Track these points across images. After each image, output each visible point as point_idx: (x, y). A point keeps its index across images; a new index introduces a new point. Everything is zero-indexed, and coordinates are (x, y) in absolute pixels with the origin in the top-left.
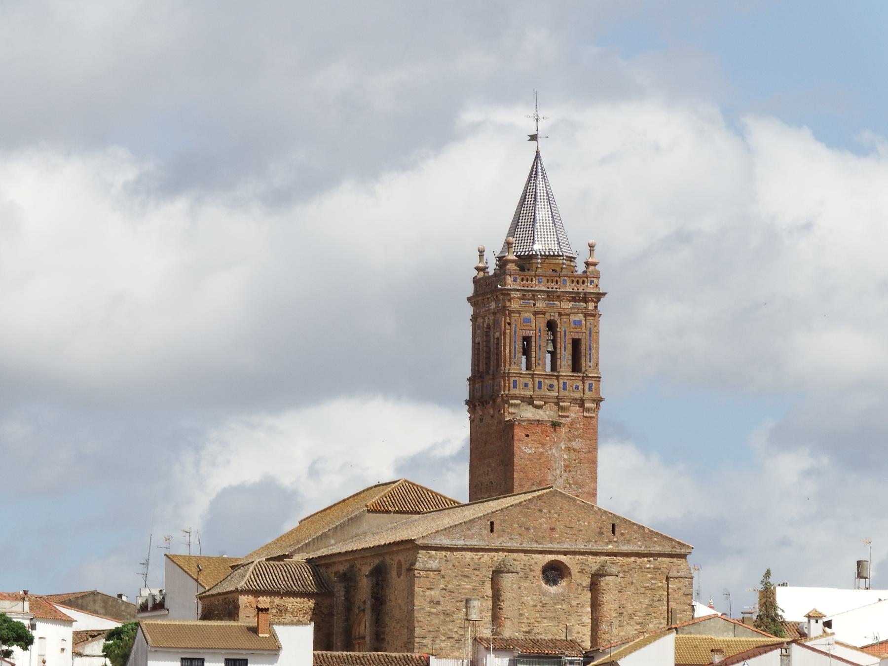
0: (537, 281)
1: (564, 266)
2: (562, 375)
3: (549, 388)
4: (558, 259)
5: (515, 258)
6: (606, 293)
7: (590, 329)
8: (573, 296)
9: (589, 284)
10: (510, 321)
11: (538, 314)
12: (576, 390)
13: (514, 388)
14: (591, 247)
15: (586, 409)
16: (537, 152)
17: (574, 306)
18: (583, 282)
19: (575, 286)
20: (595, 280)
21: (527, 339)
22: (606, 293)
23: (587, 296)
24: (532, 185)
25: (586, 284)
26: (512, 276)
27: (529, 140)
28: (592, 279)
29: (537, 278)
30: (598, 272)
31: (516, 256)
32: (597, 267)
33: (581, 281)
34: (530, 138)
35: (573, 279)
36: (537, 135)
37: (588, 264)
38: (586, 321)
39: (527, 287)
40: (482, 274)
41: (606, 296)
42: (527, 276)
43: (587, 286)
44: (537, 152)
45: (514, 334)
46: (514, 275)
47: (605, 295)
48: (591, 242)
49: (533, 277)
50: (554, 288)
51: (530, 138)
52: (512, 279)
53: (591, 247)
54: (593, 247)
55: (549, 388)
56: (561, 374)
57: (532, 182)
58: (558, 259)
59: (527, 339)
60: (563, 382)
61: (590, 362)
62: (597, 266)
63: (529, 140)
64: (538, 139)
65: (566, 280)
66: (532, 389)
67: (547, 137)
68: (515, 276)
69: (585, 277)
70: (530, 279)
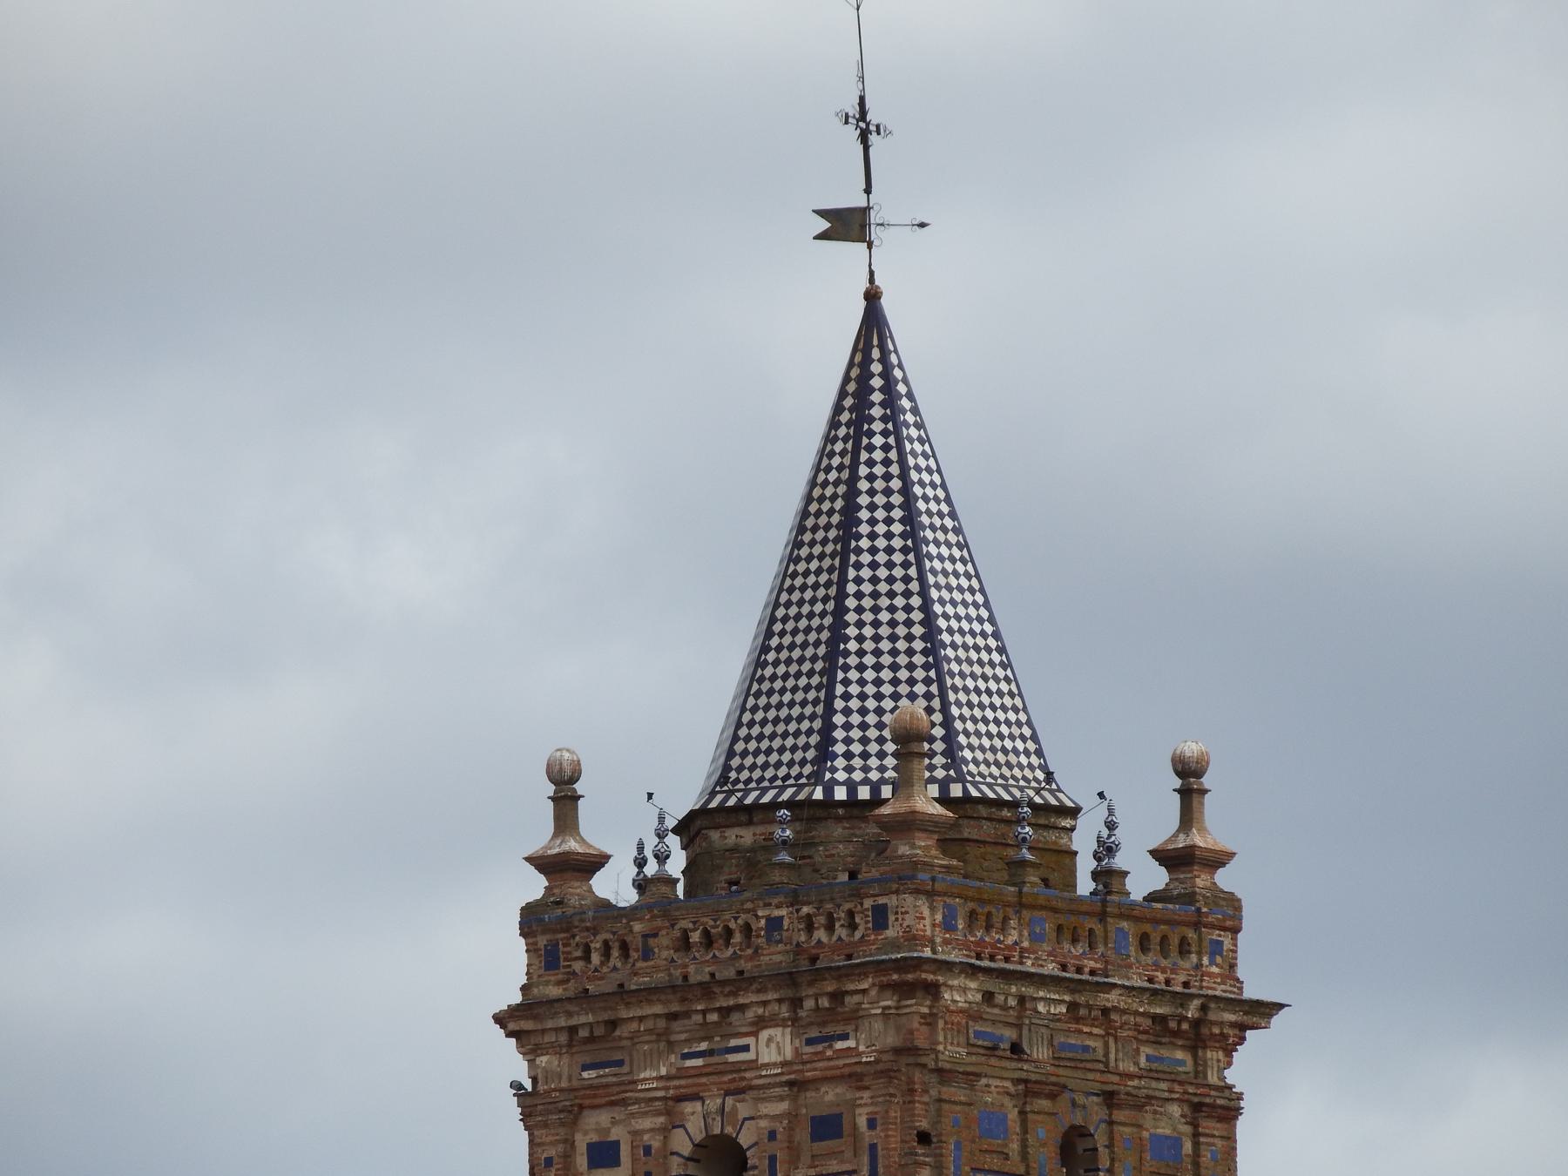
5: (938, 809)
8: (1159, 1011)
9: (1205, 961)
10: (936, 1123)
14: (1189, 775)
16: (872, 297)
18: (1184, 949)
19: (1157, 966)
23: (1212, 1016)
24: (878, 455)
25: (1194, 957)
26: (939, 904)
27: (823, 236)
28: (1215, 935)
29: (1026, 914)
33: (1176, 941)
34: (824, 225)
35: (1148, 928)
36: (868, 208)
38: (1196, 1145)
40: (767, 901)
41: (1277, 1020)
42: (990, 902)
44: (872, 297)
46: (945, 894)
47: (1271, 1016)
48: (1191, 749)
49: (1010, 911)
51: (824, 225)
52: (939, 917)
53: (1189, 775)
54: (1199, 774)
57: (878, 441)
63: (823, 236)
64: (874, 233)
67: (922, 225)
68: (948, 900)
70: (997, 920)
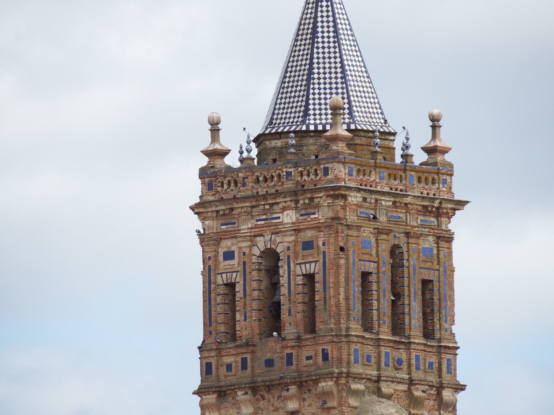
0: (378, 176)
1: (378, 149)
2: (415, 343)
3: (396, 365)
4: (388, 140)
5: (347, 133)
6: (468, 202)
7: (324, 252)
8: (425, 204)
9: (441, 186)
11: (382, 233)
12: (430, 370)
13: (355, 363)
14: (435, 122)
15: (445, 404)
17: (423, 223)
18: (433, 183)
20: (448, 178)
21: (365, 275)
22: (468, 202)
23: (443, 206)
24: (324, 9)
25: (437, 185)
28: (444, 177)
30: (451, 165)
31: (349, 130)
32: (448, 157)
35: (420, 174)
37: (430, 151)
38: (438, 250)
39: (366, 186)
41: (466, 207)
42: (365, 166)
43: (438, 188)
45: (412, 272)
46: (349, 163)
48: (436, 112)
49: (372, 169)
50: (399, 189)
52: (347, 171)
53: (435, 122)
55: (396, 365)
56: (412, 340)
58: (388, 140)
59: (365, 275)
60: (416, 356)
61: (446, 322)
62: (446, 155)
65: (413, 177)
66: (375, 366)
68: (350, 165)
69: (435, 173)
70: (367, 172)
